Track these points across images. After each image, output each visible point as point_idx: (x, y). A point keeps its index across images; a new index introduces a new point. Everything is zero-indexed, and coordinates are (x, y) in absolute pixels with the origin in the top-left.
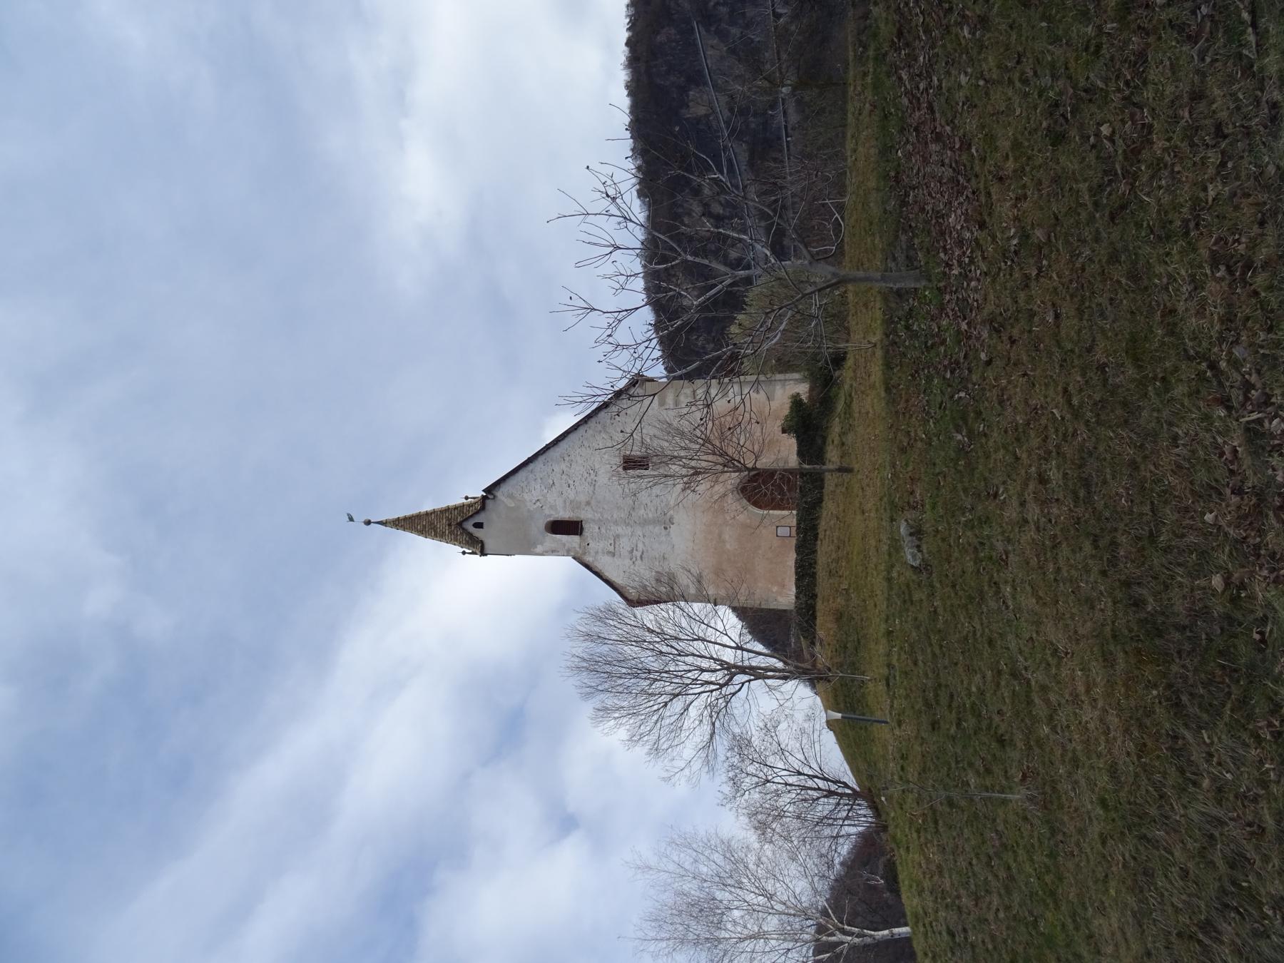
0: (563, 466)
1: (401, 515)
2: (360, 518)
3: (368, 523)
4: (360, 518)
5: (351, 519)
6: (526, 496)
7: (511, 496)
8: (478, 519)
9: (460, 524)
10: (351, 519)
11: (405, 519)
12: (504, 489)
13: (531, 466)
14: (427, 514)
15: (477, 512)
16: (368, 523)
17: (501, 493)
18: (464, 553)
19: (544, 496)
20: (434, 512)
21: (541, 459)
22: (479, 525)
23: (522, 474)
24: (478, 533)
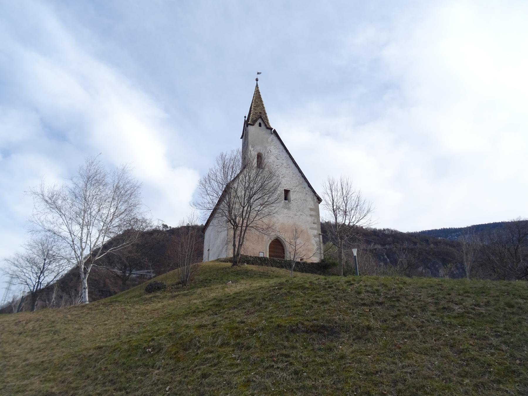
0: (285, 164)
1: (261, 94)
2: (259, 76)
3: (257, 80)
4: (259, 76)
5: (258, 73)
6: (273, 147)
7: (272, 141)
8: (262, 125)
9: (261, 117)
10: (258, 73)
11: (260, 98)
12: (275, 139)
13: (285, 151)
14: (263, 105)
15: (266, 125)
16: (257, 80)
17: (273, 136)
18: (245, 117)
19: (273, 154)
20: (264, 108)
21: (288, 156)
22: (260, 125)
23: (281, 147)
24: (257, 124)
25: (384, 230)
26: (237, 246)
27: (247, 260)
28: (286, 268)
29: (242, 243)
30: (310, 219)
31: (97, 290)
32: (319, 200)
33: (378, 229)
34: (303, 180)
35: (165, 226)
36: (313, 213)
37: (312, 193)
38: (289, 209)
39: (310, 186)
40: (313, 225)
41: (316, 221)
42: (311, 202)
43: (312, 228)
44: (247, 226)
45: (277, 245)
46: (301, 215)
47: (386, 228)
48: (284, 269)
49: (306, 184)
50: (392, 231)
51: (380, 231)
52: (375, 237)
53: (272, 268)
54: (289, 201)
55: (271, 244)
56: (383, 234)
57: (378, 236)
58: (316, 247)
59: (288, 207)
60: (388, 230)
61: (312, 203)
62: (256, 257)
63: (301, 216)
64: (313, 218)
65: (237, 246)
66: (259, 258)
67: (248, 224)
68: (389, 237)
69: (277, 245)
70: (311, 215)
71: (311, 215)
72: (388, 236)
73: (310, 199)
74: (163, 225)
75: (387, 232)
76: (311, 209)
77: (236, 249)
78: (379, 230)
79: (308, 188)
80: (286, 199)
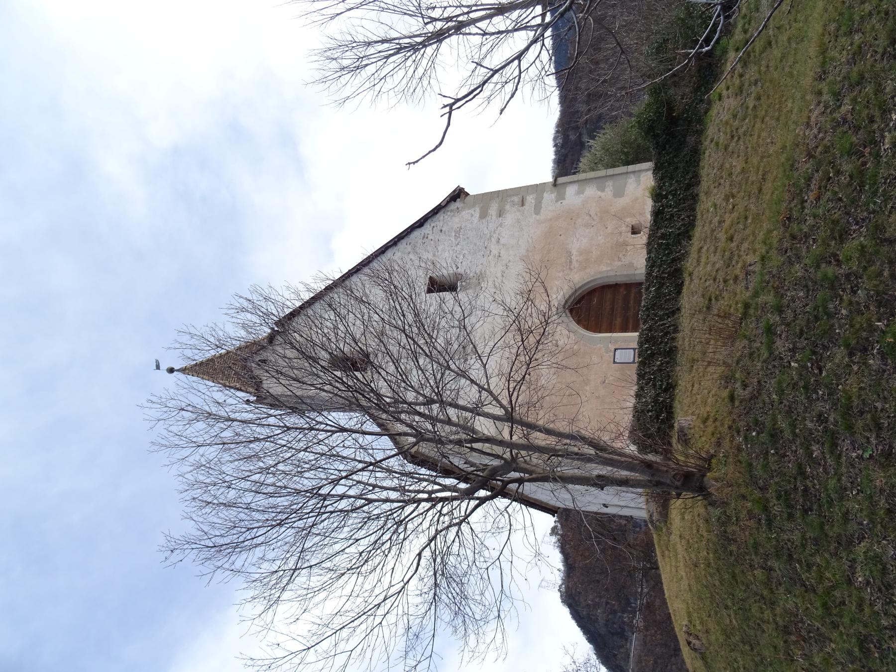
2: (164, 366)
3: (171, 370)
4: (164, 366)
5: (158, 367)
10: (158, 367)
16: (171, 370)
25: (556, 145)
26: (605, 471)
27: (655, 415)
28: (680, 259)
29: (591, 443)
30: (510, 217)
31: (673, 659)
32: (458, 195)
33: (553, 157)
34: (404, 241)
35: (554, 531)
36: (493, 210)
37: (441, 216)
38: (480, 277)
39: (420, 224)
40: (526, 207)
41: (516, 199)
42: (464, 217)
43: (537, 209)
44: (510, 418)
45: (593, 307)
46: (498, 241)
47: (551, 143)
48: (689, 264)
49: (416, 233)
50: (557, 132)
51: (557, 153)
52: (568, 161)
53: (685, 312)
54: (458, 277)
55: (587, 328)
56: (562, 146)
57: (566, 156)
58: (591, 191)
59: (474, 281)
60: (555, 139)
61: (465, 214)
62: (641, 376)
63: (502, 241)
64: (508, 207)
65: (605, 471)
66: (642, 364)
67: (500, 412)
68: (568, 136)
69: (593, 307)
70: (500, 214)
71: (500, 214)
72: (566, 139)
73: (456, 219)
74: (551, 534)
75: (560, 141)
76: (484, 215)
77: (624, 473)
78: (556, 155)
79: (427, 228)
80: (452, 288)
